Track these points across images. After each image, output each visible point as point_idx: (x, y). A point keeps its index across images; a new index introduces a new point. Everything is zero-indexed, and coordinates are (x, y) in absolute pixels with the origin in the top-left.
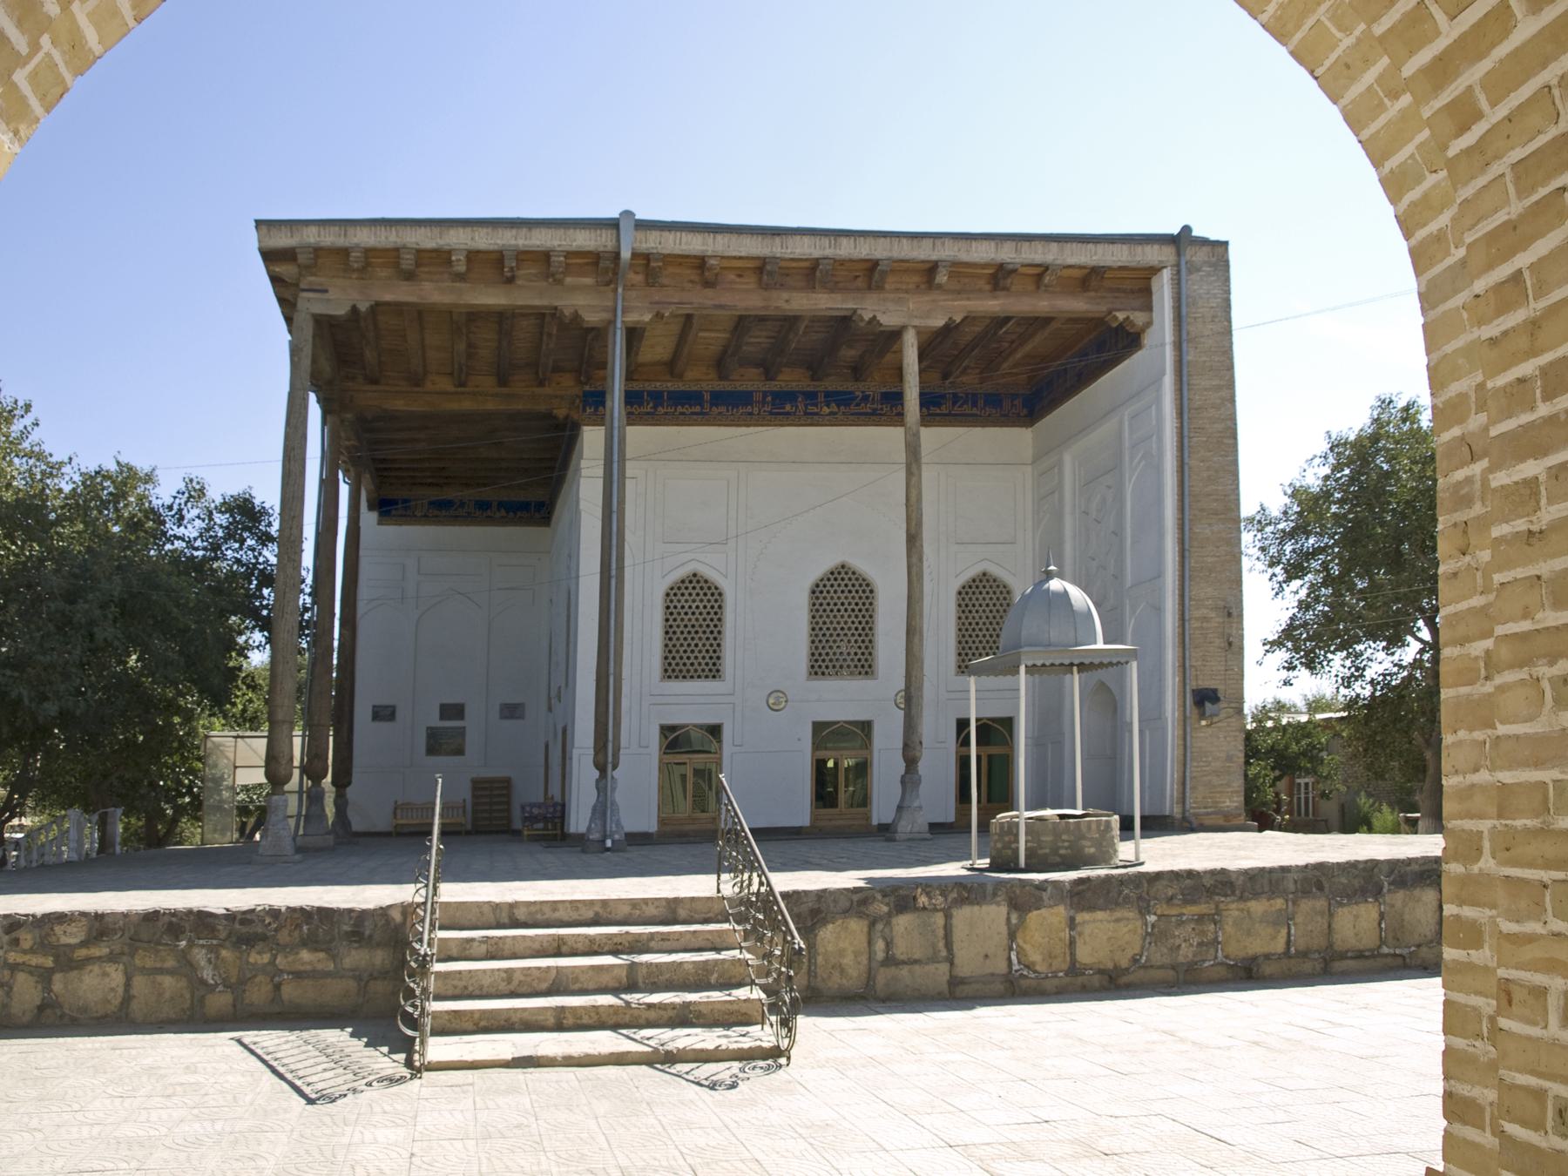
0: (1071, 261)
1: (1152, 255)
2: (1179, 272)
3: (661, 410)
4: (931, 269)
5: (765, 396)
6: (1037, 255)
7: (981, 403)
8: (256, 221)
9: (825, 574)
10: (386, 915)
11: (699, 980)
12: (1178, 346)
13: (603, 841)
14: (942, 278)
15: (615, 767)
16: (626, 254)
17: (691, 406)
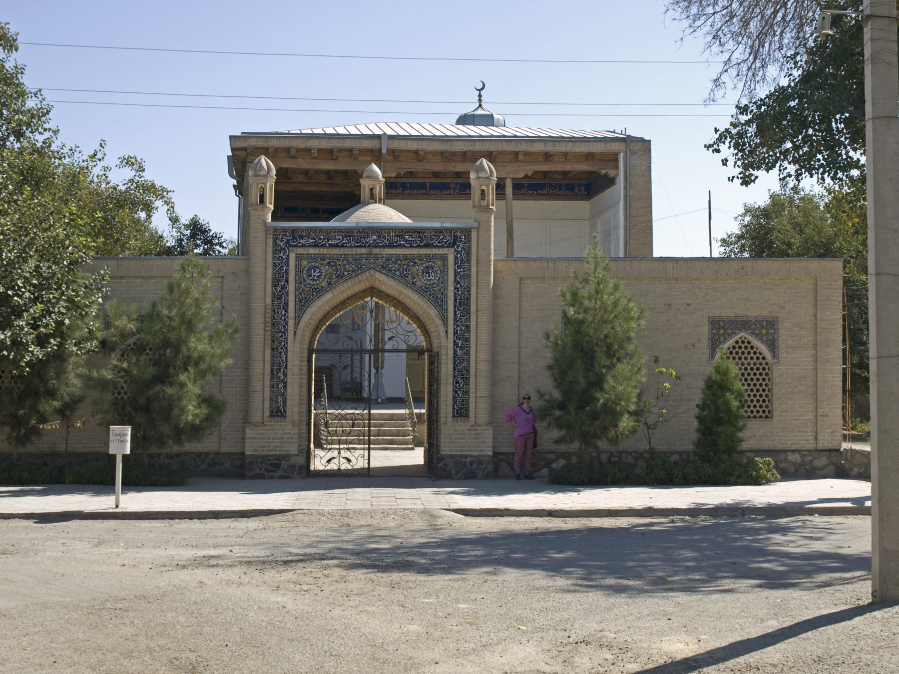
0: (578, 150)
1: (615, 147)
2: (626, 155)
3: (406, 192)
4: (517, 154)
5: (456, 185)
6: (563, 148)
7: (563, 188)
8: (231, 137)
11: (397, 434)
12: (625, 188)
13: (377, 400)
14: (521, 157)
15: (382, 368)
16: (384, 151)
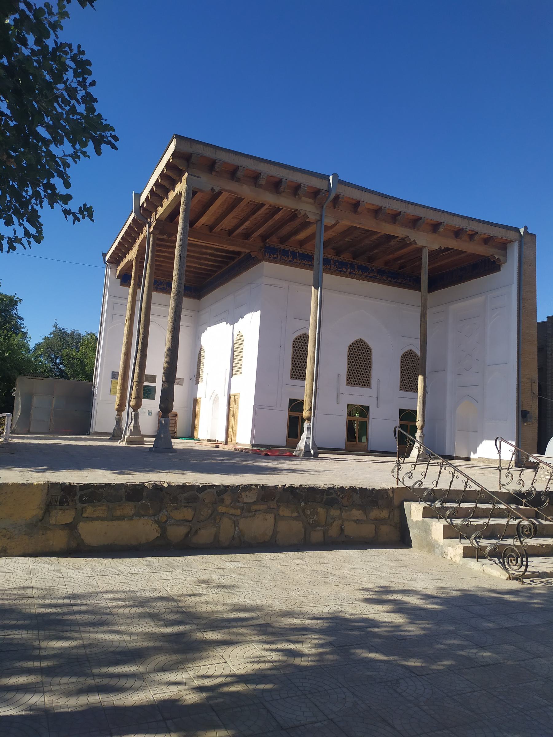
3: (295, 260)
9: (363, 340)
10: (387, 493)
14: (441, 229)
17: (307, 261)
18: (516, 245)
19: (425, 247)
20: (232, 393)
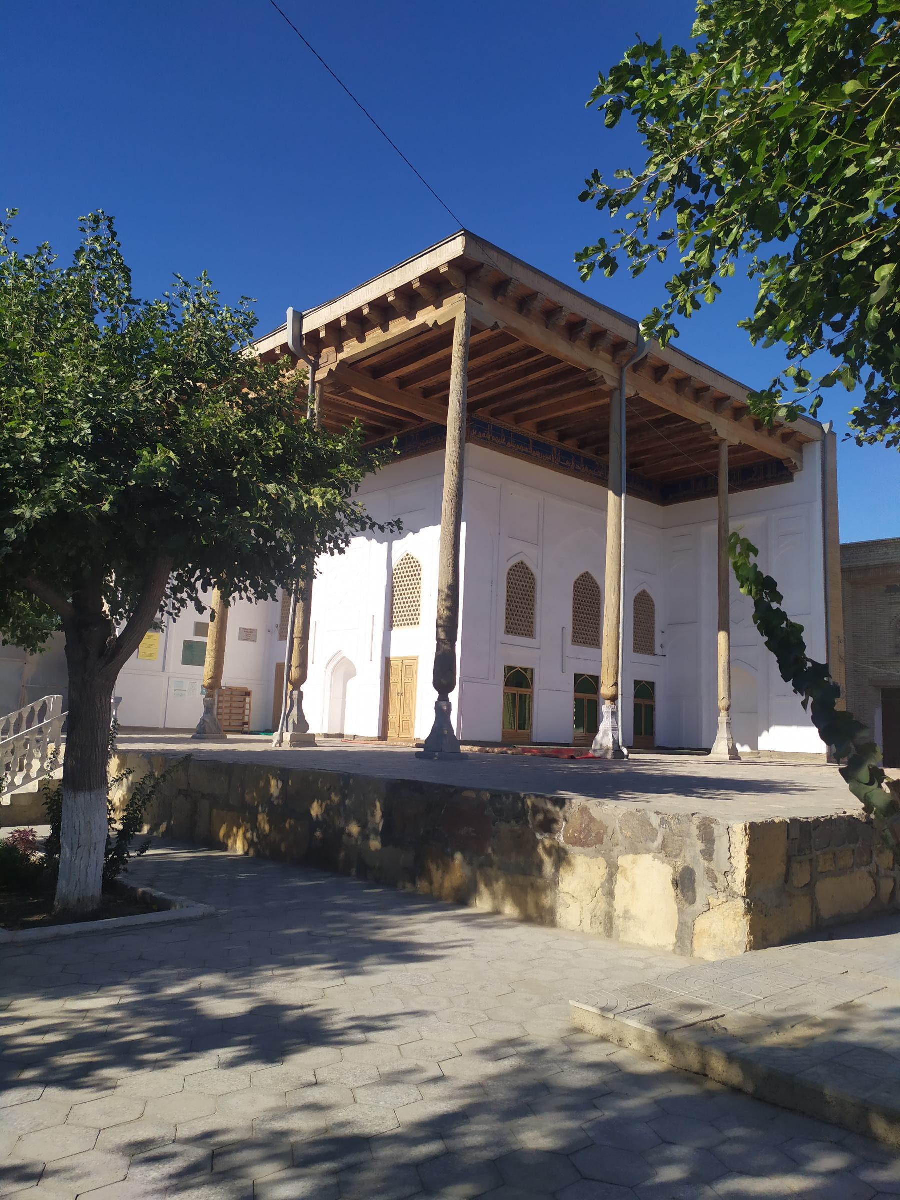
18: (818, 446)
19: (725, 440)
20: (394, 654)
